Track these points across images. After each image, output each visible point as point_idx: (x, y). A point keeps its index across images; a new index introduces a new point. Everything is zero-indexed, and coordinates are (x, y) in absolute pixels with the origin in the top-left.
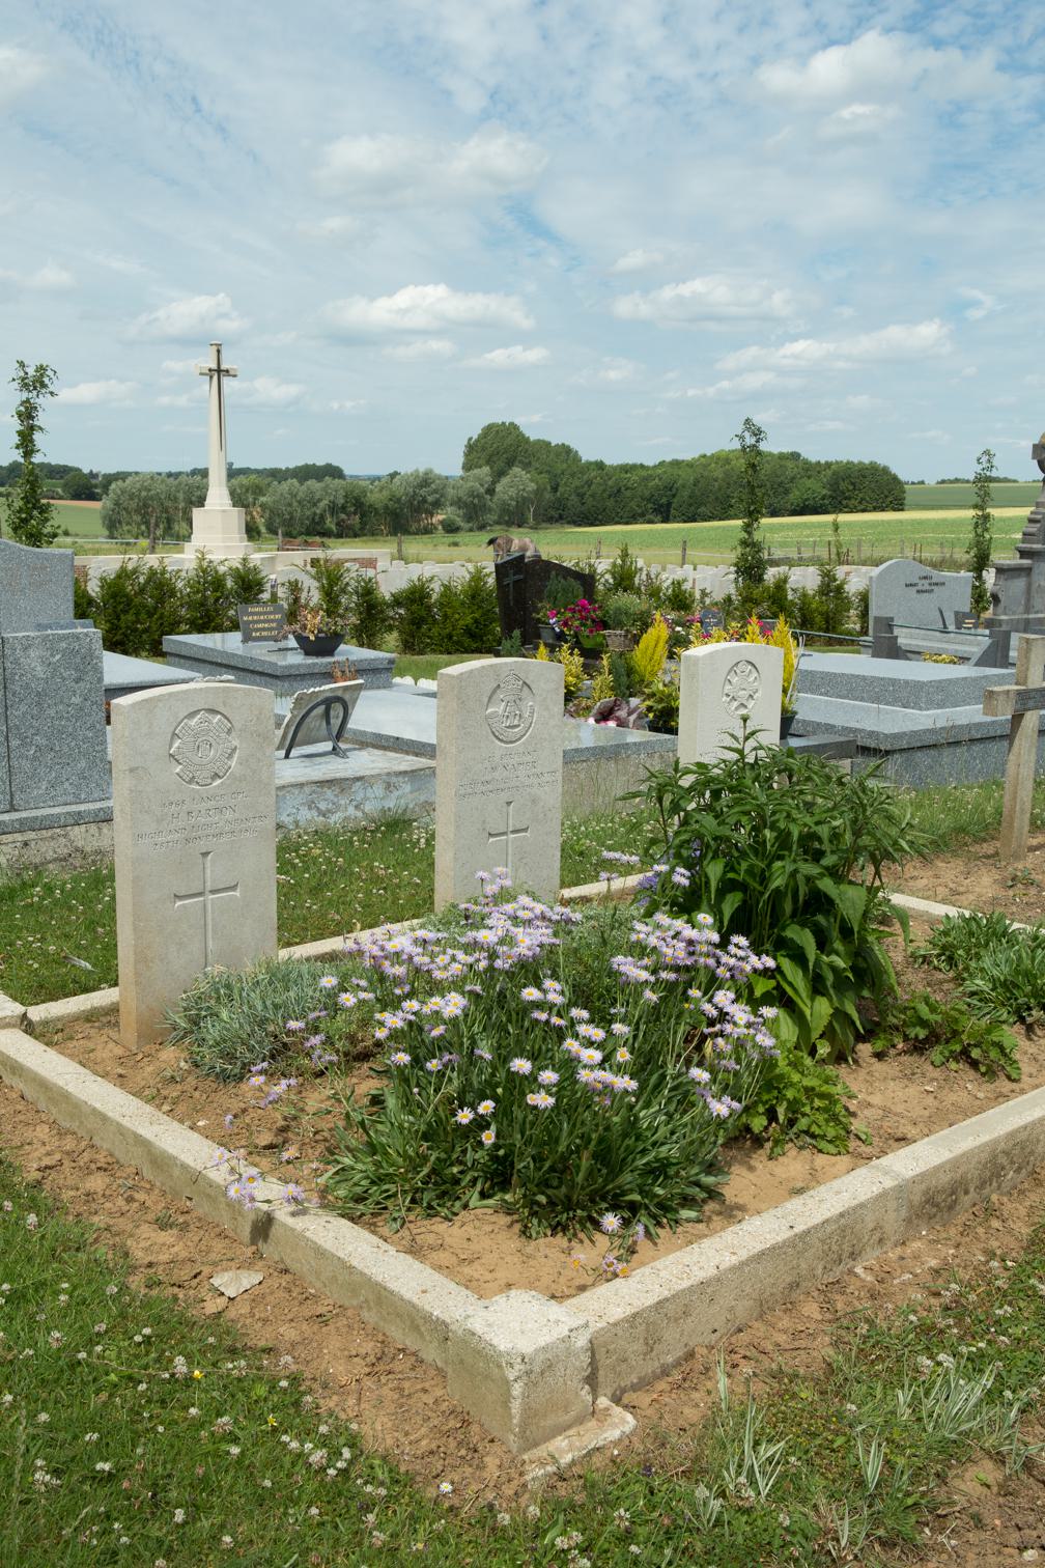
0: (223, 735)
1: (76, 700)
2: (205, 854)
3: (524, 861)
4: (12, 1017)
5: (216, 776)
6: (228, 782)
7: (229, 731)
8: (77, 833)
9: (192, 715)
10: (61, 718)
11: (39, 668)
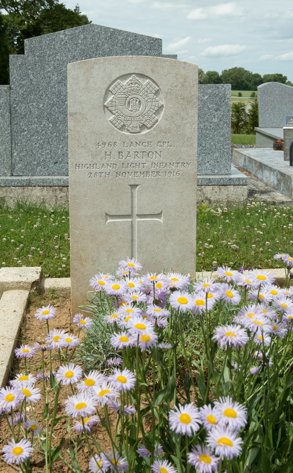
0: (151, 96)
1: (215, 120)
2: (134, 186)
4: (25, 282)
5: (143, 127)
6: (155, 132)
7: (157, 93)
9: (124, 77)
10: (207, 129)
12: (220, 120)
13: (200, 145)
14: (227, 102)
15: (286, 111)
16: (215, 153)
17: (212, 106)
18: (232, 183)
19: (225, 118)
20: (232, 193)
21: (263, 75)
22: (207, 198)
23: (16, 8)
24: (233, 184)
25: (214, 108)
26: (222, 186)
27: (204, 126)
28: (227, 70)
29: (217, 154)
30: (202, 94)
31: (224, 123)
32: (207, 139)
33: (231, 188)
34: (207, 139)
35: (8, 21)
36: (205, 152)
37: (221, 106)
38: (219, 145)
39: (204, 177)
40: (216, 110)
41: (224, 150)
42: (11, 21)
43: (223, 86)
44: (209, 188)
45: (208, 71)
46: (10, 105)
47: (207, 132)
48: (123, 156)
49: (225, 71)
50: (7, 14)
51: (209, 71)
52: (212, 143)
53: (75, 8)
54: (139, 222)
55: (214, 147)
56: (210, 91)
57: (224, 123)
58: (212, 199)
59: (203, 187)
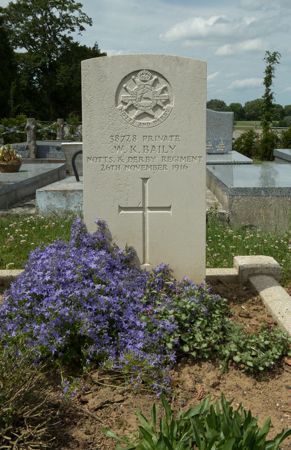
15: (212, 135)
21: (285, 106)
23: (35, 47)
28: (249, 102)
35: (25, 59)
42: (28, 59)
45: (232, 103)
48: (148, 150)
49: (248, 103)
50: (26, 52)
51: (232, 103)
53: (94, 46)
54: (149, 213)
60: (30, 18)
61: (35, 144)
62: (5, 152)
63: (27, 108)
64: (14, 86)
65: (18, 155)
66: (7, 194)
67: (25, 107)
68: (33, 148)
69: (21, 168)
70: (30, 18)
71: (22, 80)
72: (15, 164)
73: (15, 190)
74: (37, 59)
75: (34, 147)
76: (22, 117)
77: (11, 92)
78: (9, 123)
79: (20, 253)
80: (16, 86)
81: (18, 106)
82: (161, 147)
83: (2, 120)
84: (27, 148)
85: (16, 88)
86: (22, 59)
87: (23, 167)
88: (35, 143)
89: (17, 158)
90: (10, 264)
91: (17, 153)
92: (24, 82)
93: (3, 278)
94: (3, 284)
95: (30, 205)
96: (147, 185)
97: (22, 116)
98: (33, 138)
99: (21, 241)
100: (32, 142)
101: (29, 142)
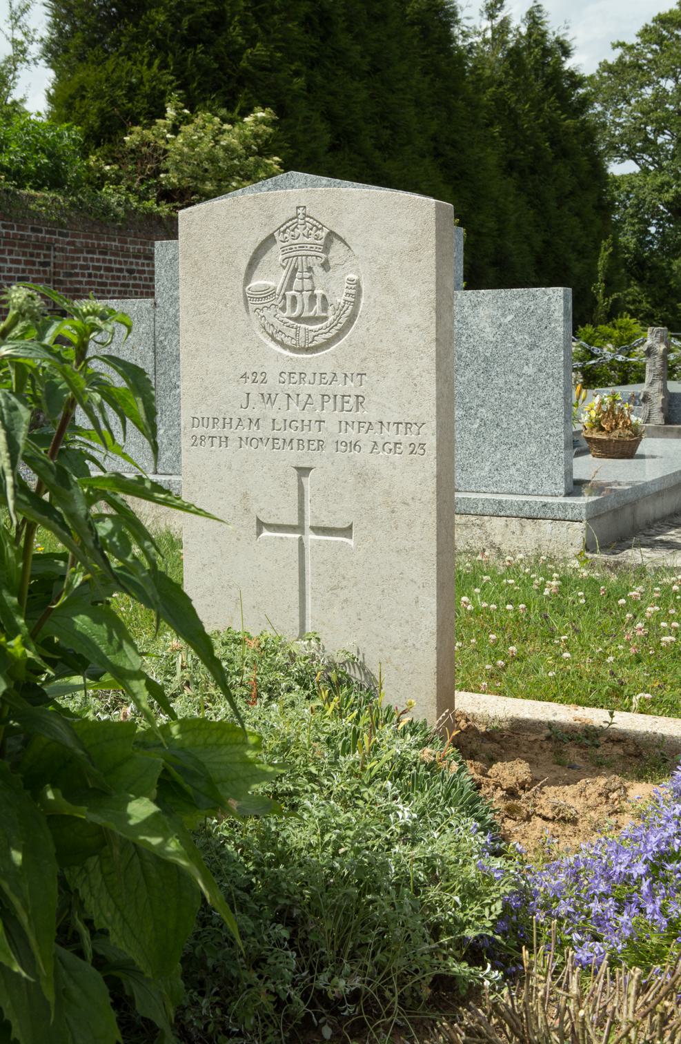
3: (343, 594)
8: (496, 524)
10: (510, 390)
11: (488, 330)
12: (540, 370)
13: (498, 425)
14: (554, 328)
16: (528, 444)
17: (521, 337)
18: (549, 515)
19: (550, 365)
20: (548, 537)
22: (492, 546)
24: (552, 516)
25: (526, 342)
26: (528, 518)
27: (506, 382)
29: (533, 448)
30: (500, 312)
31: (549, 376)
32: (512, 412)
33: (547, 526)
34: (512, 412)
36: (507, 440)
37: (541, 338)
38: (537, 427)
39: (488, 496)
40: (532, 347)
41: (547, 437)
43: (545, 293)
44: (498, 523)
46: (154, 337)
47: (512, 396)
52: (522, 423)
55: (527, 431)
56: (517, 303)
57: (549, 376)
58: (503, 547)
59: (486, 518)
60: (648, 92)
61: (664, 390)
62: (604, 408)
63: (634, 302)
64: (606, 250)
65: (634, 418)
66: (615, 512)
67: (629, 298)
68: (658, 400)
69: (639, 451)
70: (648, 92)
71: (625, 234)
72: (628, 439)
73: (633, 504)
74: (663, 184)
75: (662, 397)
76: (628, 323)
77: (601, 264)
78: (597, 337)
79: (663, 669)
80: (611, 249)
81: (615, 296)
82: (205, 420)
83: (581, 329)
84: (646, 399)
85: (610, 254)
86: (625, 187)
87: (645, 446)
88: (665, 386)
89: (631, 425)
90: (641, 695)
91: (631, 411)
92: (628, 239)
93: (637, 735)
94: (641, 754)
95: (668, 542)
96: (307, 481)
97: (627, 320)
98: (661, 374)
99: (663, 639)
100: (658, 385)
101: (651, 384)
